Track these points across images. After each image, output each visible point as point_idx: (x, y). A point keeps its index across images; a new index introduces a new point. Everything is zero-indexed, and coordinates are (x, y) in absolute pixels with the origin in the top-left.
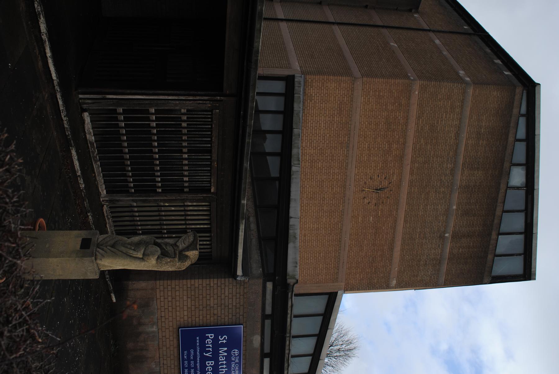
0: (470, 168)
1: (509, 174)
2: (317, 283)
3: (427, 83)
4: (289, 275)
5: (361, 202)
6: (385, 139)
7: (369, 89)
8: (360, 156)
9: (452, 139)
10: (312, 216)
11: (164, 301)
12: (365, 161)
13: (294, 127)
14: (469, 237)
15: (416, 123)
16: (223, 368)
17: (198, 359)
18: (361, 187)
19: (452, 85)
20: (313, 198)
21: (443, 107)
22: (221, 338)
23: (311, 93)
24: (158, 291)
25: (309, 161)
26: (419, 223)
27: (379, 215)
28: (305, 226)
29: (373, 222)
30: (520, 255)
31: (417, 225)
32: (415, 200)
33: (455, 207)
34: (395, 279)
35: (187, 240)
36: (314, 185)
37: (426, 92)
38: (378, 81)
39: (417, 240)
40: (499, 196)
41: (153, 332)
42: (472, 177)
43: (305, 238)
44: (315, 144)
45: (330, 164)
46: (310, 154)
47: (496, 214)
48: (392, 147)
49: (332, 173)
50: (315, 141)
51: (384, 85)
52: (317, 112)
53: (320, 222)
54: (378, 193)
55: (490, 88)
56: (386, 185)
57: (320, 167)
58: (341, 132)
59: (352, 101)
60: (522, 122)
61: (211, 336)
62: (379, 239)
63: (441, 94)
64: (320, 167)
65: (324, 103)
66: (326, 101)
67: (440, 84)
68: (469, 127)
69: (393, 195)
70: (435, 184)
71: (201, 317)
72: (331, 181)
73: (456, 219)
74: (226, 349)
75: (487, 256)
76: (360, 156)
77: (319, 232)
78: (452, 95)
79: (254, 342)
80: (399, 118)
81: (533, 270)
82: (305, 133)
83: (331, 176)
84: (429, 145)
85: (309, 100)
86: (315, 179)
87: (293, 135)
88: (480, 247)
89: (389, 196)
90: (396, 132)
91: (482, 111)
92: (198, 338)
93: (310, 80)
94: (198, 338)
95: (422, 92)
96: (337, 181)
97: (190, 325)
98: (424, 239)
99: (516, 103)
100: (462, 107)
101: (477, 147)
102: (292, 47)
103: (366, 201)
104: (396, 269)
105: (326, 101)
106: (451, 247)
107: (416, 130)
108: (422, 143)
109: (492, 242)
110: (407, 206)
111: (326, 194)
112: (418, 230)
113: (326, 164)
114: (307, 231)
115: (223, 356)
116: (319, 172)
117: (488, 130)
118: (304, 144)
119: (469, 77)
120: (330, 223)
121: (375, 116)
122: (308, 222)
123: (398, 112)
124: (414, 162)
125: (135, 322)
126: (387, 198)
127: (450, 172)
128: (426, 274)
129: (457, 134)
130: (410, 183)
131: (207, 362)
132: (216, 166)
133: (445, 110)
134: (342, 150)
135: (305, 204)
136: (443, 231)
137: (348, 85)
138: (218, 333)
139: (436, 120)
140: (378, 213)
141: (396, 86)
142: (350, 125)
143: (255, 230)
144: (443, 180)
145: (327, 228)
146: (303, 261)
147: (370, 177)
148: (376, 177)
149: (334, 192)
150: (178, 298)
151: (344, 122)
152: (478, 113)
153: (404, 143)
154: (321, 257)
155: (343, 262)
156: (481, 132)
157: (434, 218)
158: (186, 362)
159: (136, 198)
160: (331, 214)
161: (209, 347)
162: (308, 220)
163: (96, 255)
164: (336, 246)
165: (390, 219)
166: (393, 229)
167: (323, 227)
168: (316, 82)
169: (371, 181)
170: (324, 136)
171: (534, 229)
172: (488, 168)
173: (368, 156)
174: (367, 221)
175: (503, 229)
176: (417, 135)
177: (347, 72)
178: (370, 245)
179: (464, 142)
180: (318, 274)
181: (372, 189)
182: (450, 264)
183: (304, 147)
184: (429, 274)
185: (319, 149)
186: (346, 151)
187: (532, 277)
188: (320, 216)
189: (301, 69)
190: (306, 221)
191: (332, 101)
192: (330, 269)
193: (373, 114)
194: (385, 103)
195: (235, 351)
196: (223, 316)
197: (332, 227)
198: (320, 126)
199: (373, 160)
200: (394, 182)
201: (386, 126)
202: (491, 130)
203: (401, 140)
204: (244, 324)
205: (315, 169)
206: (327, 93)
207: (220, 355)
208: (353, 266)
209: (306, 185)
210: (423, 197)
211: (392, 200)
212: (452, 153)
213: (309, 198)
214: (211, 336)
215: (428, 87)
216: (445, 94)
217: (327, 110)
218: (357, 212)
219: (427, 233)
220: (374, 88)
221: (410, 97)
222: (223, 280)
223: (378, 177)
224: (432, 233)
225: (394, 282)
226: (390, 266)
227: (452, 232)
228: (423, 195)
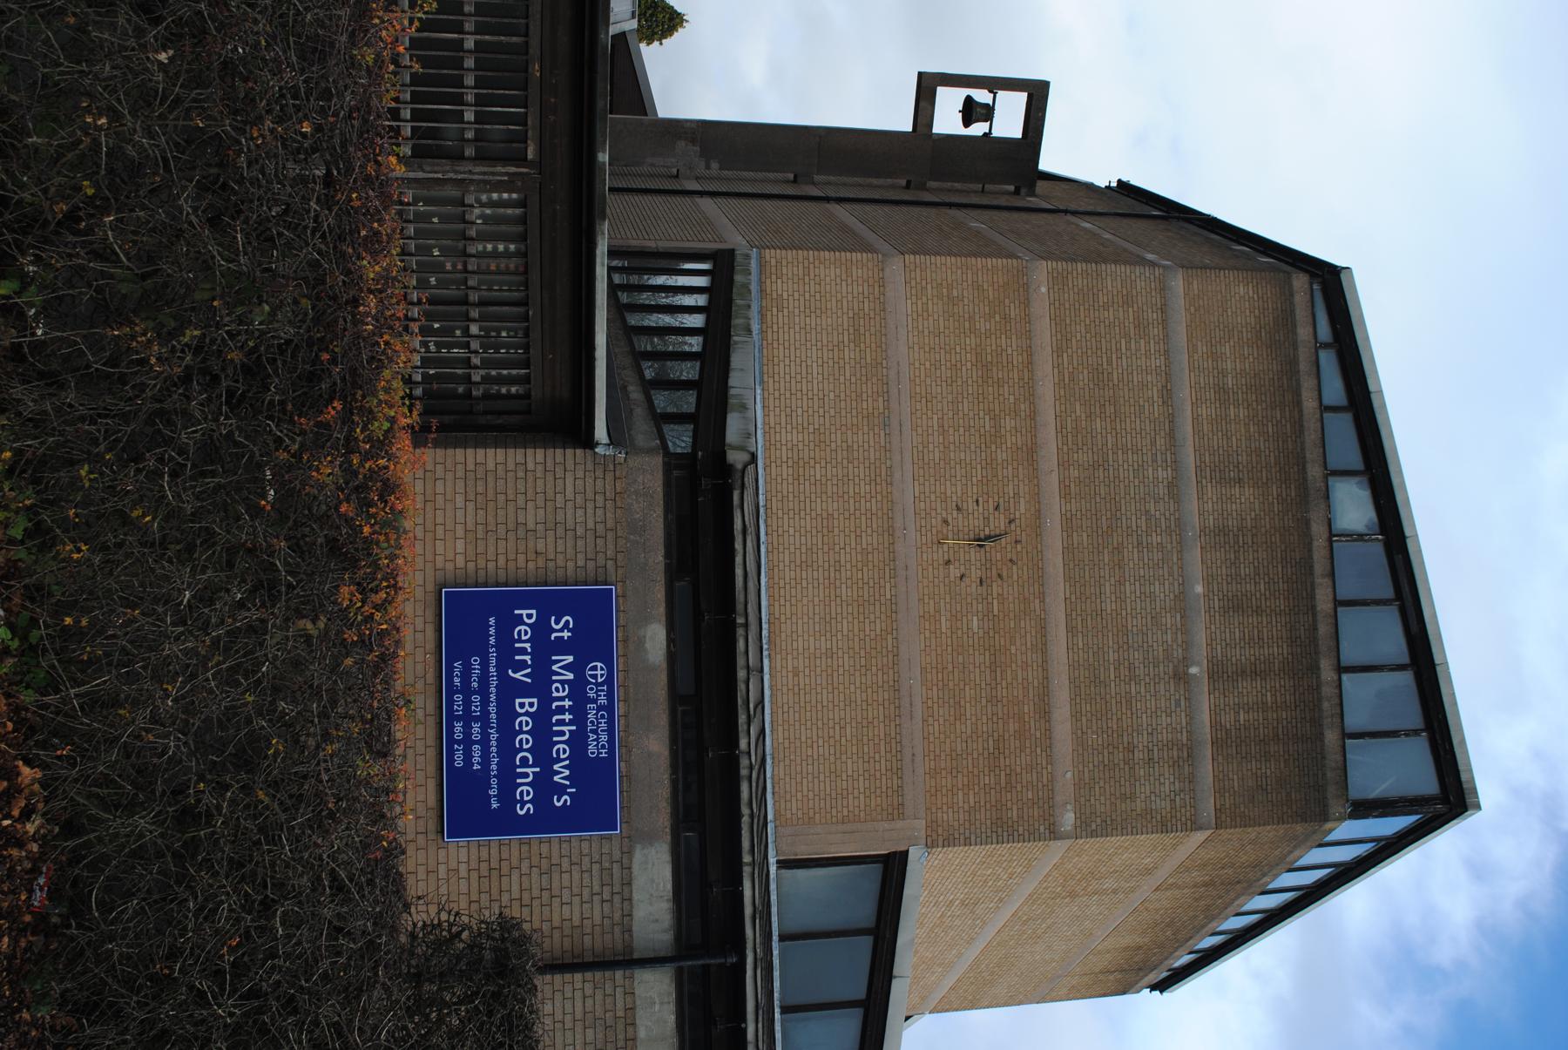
0: (1218, 479)
8: (920, 448)
10: (811, 615)
12: (937, 461)
16: (561, 723)
17: (493, 690)
18: (934, 530)
20: (809, 563)
22: (557, 622)
23: (780, 292)
25: (790, 464)
26: (1110, 634)
27: (996, 612)
29: (981, 631)
31: (1105, 642)
32: (1087, 568)
33: (1199, 589)
34: (1069, 807)
36: (808, 529)
39: (1113, 684)
43: (796, 678)
44: (800, 419)
45: (845, 471)
47: (1319, 609)
48: (1003, 425)
49: (851, 494)
50: (800, 410)
51: (959, 272)
52: (798, 338)
54: (983, 549)
56: (1003, 528)
57: (818, 477)
60: (1328, 360)
61: (529, 615)
64: (818, 477)
66: (818, 311)
68: (1192, 374)
74: (570, 659)
77: (835, 663)
79: (648, 645)
80: (1009, 352)
81: (1464, 777)
82: (771, 391)
83: (852, 501)
85: (775, 309)
86: (808, 511)
89: (1014, 558)
92: (492, 621)
94: (492, 621)
95: (1056, 287)
96: (869, 515)
98: (1133, 683)
99: (1301, 313)
100: (1164, 323)
103: (954, 572)
104: (1069, 775)
106: (1213, 708)
108: (1078, 413)
110: (1067, 587)
112: (1112, 656)
113: (834, 470)
114: (801, 661)
115: (562, 682)
120: (862, 637)
121: (947, 347)
122: (800, 632)
124: (1066, 465)
126: (1010, 564)
127: (1166, 492)
128: (1157, 791)
130: (1064, 523)
131: (518, 701)
132: (538, 74)
135: (787, 581)
136: (1180, 657)
137: (870, 273)
140: (990, 606)
145: (857, 649)
146: (798, 750)
147: (954, 504)
148: (971, 506)
150: (440, 499)
151: (869, 361)
152: (1208, 339)
153: (1033, 415)
154: (849, 738)
155: (913, 755)
157: (1149, 618)
158: (458, 698)
161: (523, 651)
164: (886, 703)
165: (1028, 622)
166: (1039, 651)
167: (845, 648)
169: (960, 515)
171: (1434, 650)
173: (942, 449)
174: (965, 630)
175: (1350, 655)
178: (984, 701)
179: (1189, 413)
180: (845, 793)
182: (1220, 757)
183: (772, 425)
188: (834, 615)
193: (942, 341)
194: (967, 316)
195: (595, 668)
196: (560, 562)
198: (810, 371)
200: (1023, 520)
202: (1253, 381)
203: (1022, 407)
205: (807, 483)
207: (554, 678)
208: (943, 766)
209: (786, 528)
210: (1106, 561)
212: (1163, 440)
213: (798, 563)
214: (530, 616)
218: (932, 602)
219: (1137, 665)
222: (559, 451)
223: (978, 505)
226: (1049, 767)
227: (1206, 661)
228: (1106, 555)
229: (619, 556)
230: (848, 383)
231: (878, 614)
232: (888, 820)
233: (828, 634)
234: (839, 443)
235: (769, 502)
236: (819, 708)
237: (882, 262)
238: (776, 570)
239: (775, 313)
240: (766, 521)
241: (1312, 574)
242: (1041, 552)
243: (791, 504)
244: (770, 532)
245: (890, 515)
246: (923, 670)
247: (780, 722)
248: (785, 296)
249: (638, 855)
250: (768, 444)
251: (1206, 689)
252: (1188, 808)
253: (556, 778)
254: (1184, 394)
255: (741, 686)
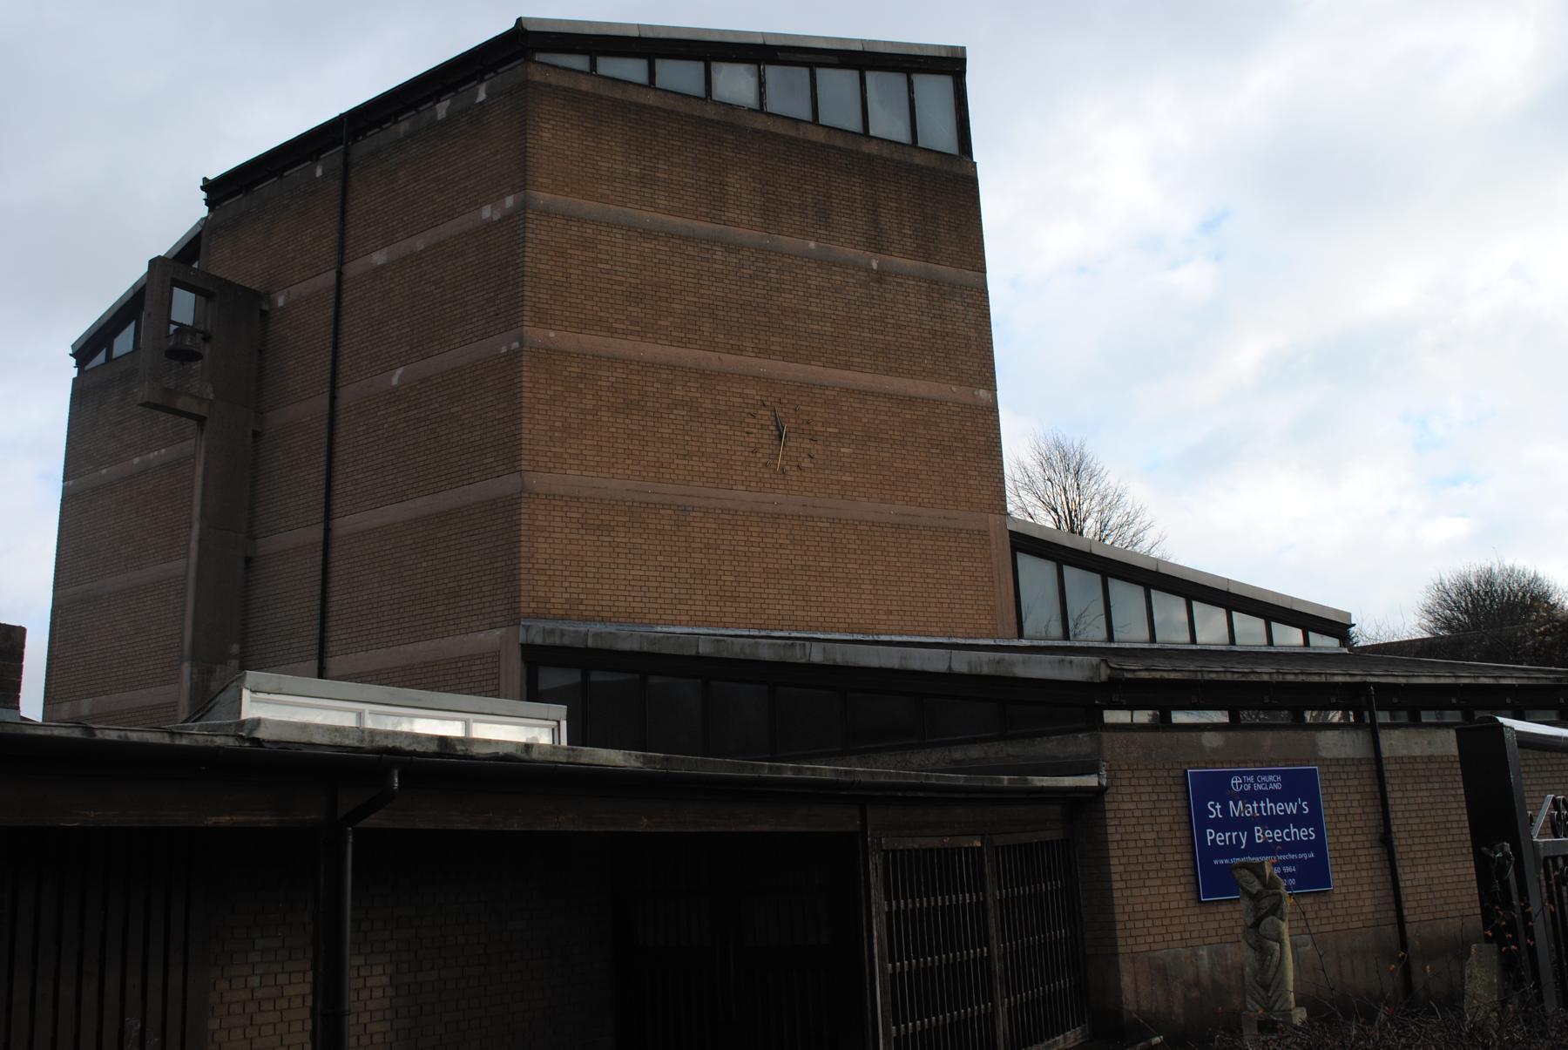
1: (730, 107)
2: (993, 582)
3: (528, 308)
4: (1092, 678)
5: (810, 475)
6: (664, 415)
7: (549, 454)
8: (704, 479)
9: (658, 247)
11: (1154, 935)
13: (693, 652)
14: (876, 211)
15: (624, 337)
16: (1265, 808)
18: (774, 476)
19: (530, 245)
20: (804, 593)
21: (583, 268)
22: (1212, 814)
23: (564, 601)
24: (1136, 949)
25: (722, 604)
27: (836, 431)
28: (867, 612)
30: (910, 85)
33: (812, 245)
34: (976, 393)
35: (1248, 878)
36: (776, 591)
37: (550, 312)
38: (527, 432)
40: (783, 132)
41: (1210, 955)
42: (743, 200)
46: (706, 603)
47: (823, 141)
49: (746, 549)
51: (537, 416)
52: (607, 587)
53: (857, 576)
54: (789, 435)
55: (534, 148)
56: (769, 413)
58: (650, 526)
59: (578, 498)
60: (611, 67)
62: (890, 432)
63: (552, 273)
65: (585, 569)
66: (582, 564)
67: (530, 274)
69: (791, 397)
70: (762, 292)
71: (1178, 857)
72: (766, 550)
73: (839, 241)
74: (1231, 803)
75: (917, 165)
76: (704, 479)
78: (553, 244)
79: (1214, 745)
81: (944, 54)
82: (658, 617)
84: (673, 305)
85: (581, 607)
87: (716, 655)
88: (897, 183)
90: (646, 388)
91: (590, 170)
92: (1216, 862)
93: (533, 605)
94: (1216, 862)
95: (549, 322)
97: (1192, 880)
99: (566, 82)
101: (672, 186)
102: (421, 646)
103: (806, 463)
105: (582, 564)
106: (902, 255)
107: (639, 339)
109: (886, 153)
111: (794, 562)
114: (879, 607)
116: (745, 579)
117: (632, 156)
118: (683, 618)
119: (502, 197)
123: (599, 383)
125: (1195, 994)
129: (646, 236)
131: (1258, 841)
133: (589, 264)
134: (693, 524)
135: (819, 614)
136: (865, 274)
138: (1205, 822)
139: (614, 287)
141: (537, 386)
142: (635, 504)
143: (986, 748)
144: (751, 272)
147: (751, 455)
149: (788, 542)
153: (673, 368)
155: (944, 518)
156: (639, 175)
159: (999, 996)
160: (839, 550)
161: (1230, 837)
162: (855, 606)
163: (1284, 1011)
167: (869, 567)
168: (536, 588)
170: (661, 569)
172: (720, 158)
173: (704, 459)
176: (650, 335)
177: (508, 507)
178: (903, 452)
179: (664, 217)
181: (778, 447)
183: (688, 618)
184: (962, 308)
185: (692, 582)
186: (694, 514)
187: (960, 56)
189: (498, 625)
190: (856, 611)
191: (579, 548)
192: (960, 549)
194: (581, 416)
195: (1235, 784)
196: (1173, 812)
197: (869, 548)
199: (714, 446)
201: (634, 412)
203: (664, 376)
204: (1185, 767)
206: (562, 561)
211: (801, 398)
213: (804, 603)
215: (538, 305)
216: (553, 263)
217: (601, 560)
218: (831, 486)
220: (546, 441)
221: (562, 352)
224: (872, 301)
225: (983, 393)
226: (949, 404)
227: (868, 253)
229: (1166, 767)
230: (648, 542)
231: (842, 536)
232: (990, 545)
233: (860, 581)
234: (703, 556)
235: (756, 626)
236: (914, 594)
237: (530, 494)
238: (810, 624)
239: (583, 607)
240: (771, 630)
241: (796, 139)
242: (788, 381)
243: (756, 606)
244: (780, 627)
245: (763, 515)
246: (883, 501)
247: (925, 629)
248: (567, 596)
249: (1324, 754)
250: (705, 623)
251: (887, 257)
252: (973, 293)
253: (1295, 812)
254: (647, 216)
255: (1236, 677)
